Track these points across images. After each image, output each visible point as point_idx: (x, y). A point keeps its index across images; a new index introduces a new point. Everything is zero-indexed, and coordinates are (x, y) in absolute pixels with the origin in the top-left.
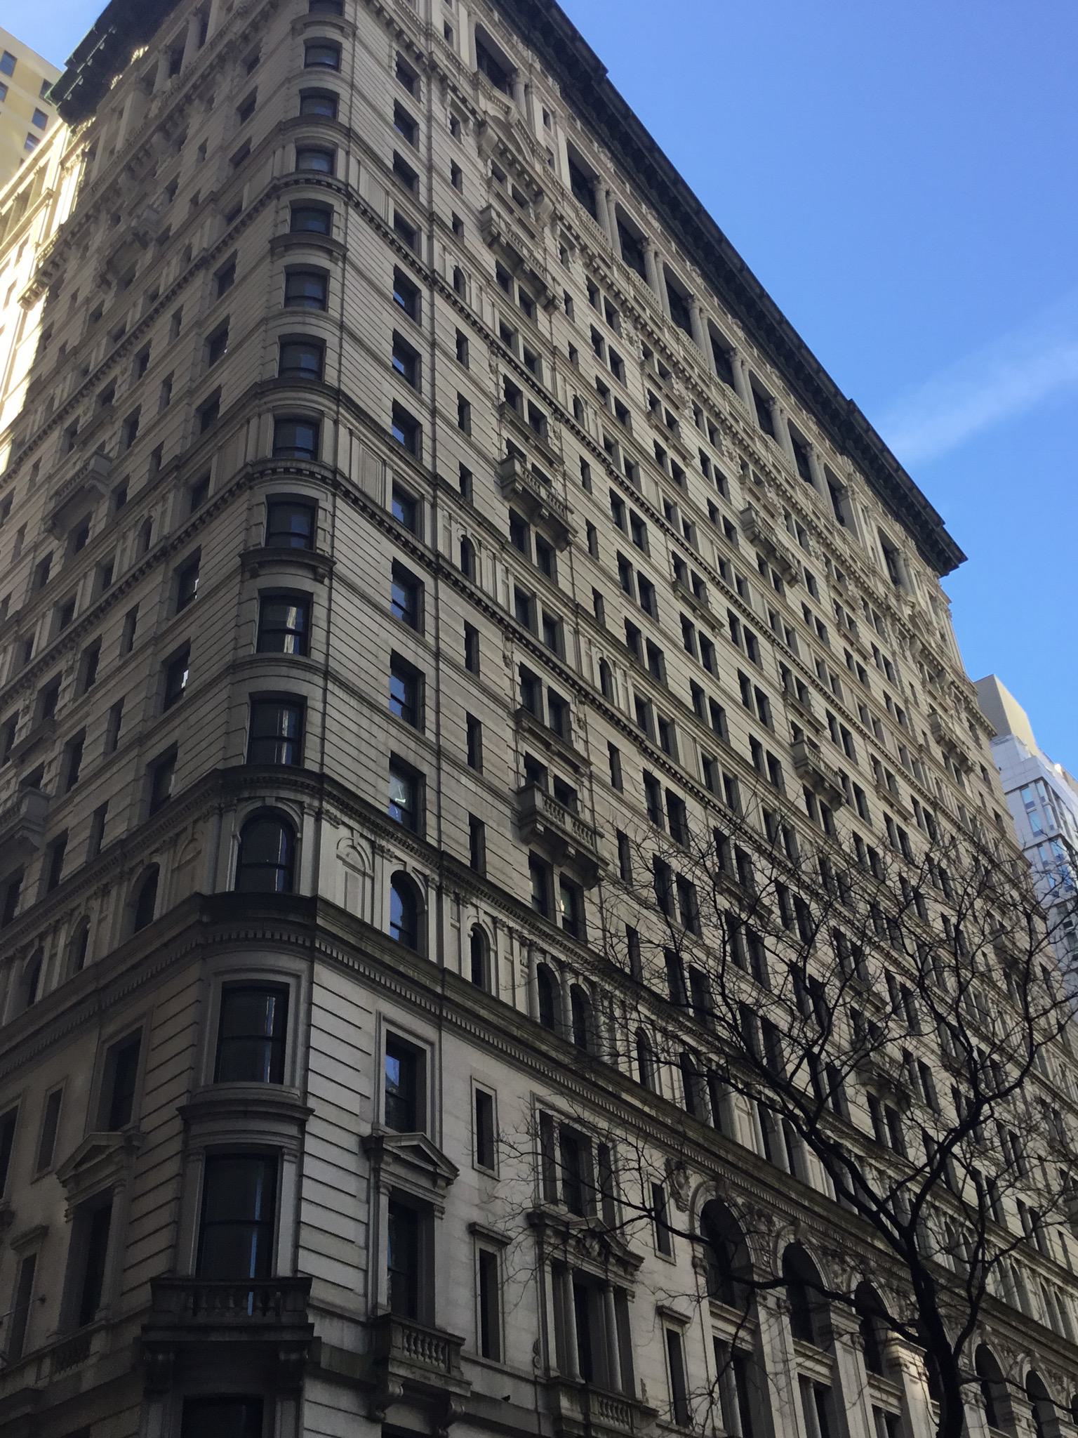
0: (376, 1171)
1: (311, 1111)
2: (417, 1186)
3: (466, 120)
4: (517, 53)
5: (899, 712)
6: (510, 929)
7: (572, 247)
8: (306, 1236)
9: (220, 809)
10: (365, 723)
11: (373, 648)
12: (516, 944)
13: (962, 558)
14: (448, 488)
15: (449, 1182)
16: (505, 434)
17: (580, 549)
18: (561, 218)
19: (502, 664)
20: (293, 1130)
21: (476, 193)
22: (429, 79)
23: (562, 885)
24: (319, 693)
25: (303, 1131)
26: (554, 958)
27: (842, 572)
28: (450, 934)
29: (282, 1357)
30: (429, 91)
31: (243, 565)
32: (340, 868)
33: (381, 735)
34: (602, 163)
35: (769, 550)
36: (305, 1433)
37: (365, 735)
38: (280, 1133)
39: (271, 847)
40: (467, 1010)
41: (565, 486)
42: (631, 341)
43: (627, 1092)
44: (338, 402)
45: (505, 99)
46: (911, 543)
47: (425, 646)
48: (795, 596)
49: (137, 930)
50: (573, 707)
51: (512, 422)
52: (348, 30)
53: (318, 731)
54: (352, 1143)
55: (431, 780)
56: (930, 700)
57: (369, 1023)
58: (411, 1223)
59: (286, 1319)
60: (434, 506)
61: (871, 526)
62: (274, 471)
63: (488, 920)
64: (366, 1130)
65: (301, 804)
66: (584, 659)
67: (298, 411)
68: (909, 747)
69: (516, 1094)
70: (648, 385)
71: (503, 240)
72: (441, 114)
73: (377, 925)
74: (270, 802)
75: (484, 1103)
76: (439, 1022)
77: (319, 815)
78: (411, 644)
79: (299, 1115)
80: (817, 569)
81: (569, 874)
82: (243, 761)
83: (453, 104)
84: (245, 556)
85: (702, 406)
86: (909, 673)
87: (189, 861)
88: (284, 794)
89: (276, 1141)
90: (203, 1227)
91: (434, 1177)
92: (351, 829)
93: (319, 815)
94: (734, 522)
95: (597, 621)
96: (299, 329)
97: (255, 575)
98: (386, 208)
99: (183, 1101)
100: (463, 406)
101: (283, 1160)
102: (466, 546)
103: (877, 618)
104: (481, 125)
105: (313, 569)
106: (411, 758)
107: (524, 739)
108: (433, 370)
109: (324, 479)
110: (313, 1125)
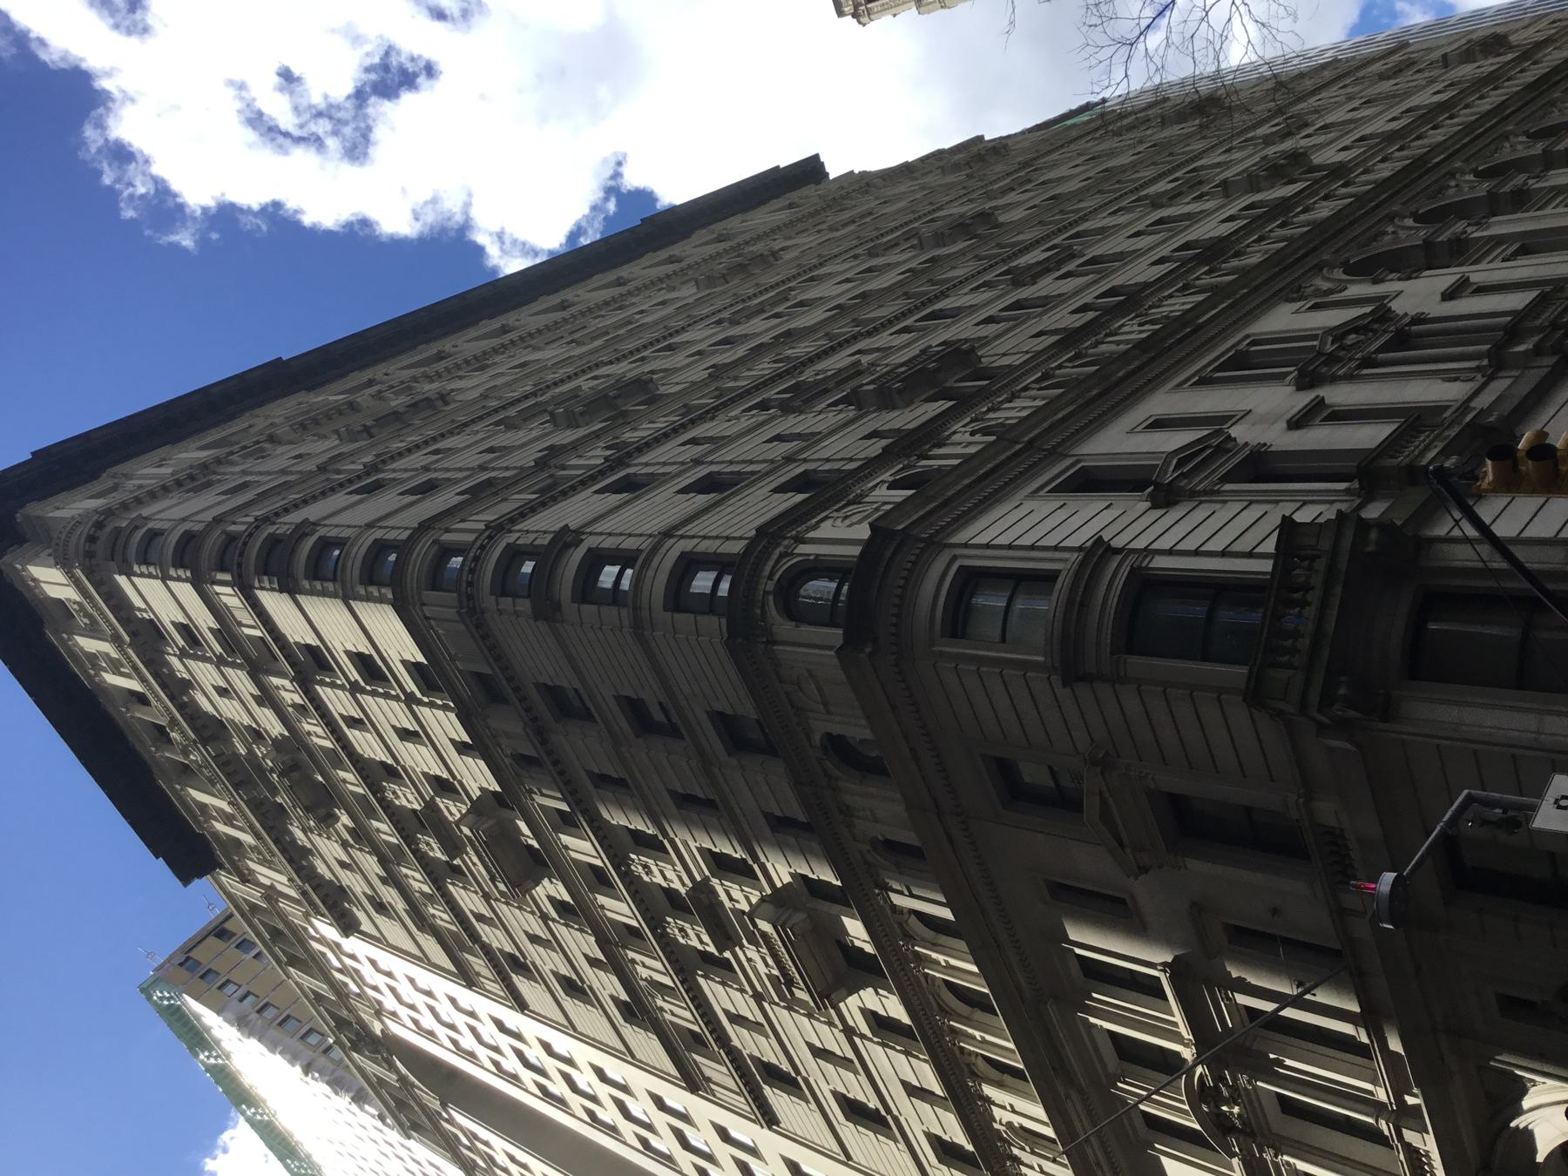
7: (410, 388)
9: (768, 642)
13: (816, 157)
22: (215, 473)
29: (1370, 548)
31: (546, 619)
38: (1115, 576)
40: (1051, 427)
41: (682, 537)
43: (1198, 317)
49: (888, 775)
52: (138, 523)
59: (1326, 545)
62: (470, 584)
65: (781, 556)
67: (425, 568)
71: (369, 423)
74: (770, 586)
82: (724, 621)
84: (538, 615)
87: (820, 689)
88: (768, 569)
90: (1206, 657)
92: (826, 518)
93: (801, 540)
96: (358, 563)
97: (558, 607)
99: (1056, 680)
101: (1147, 568)
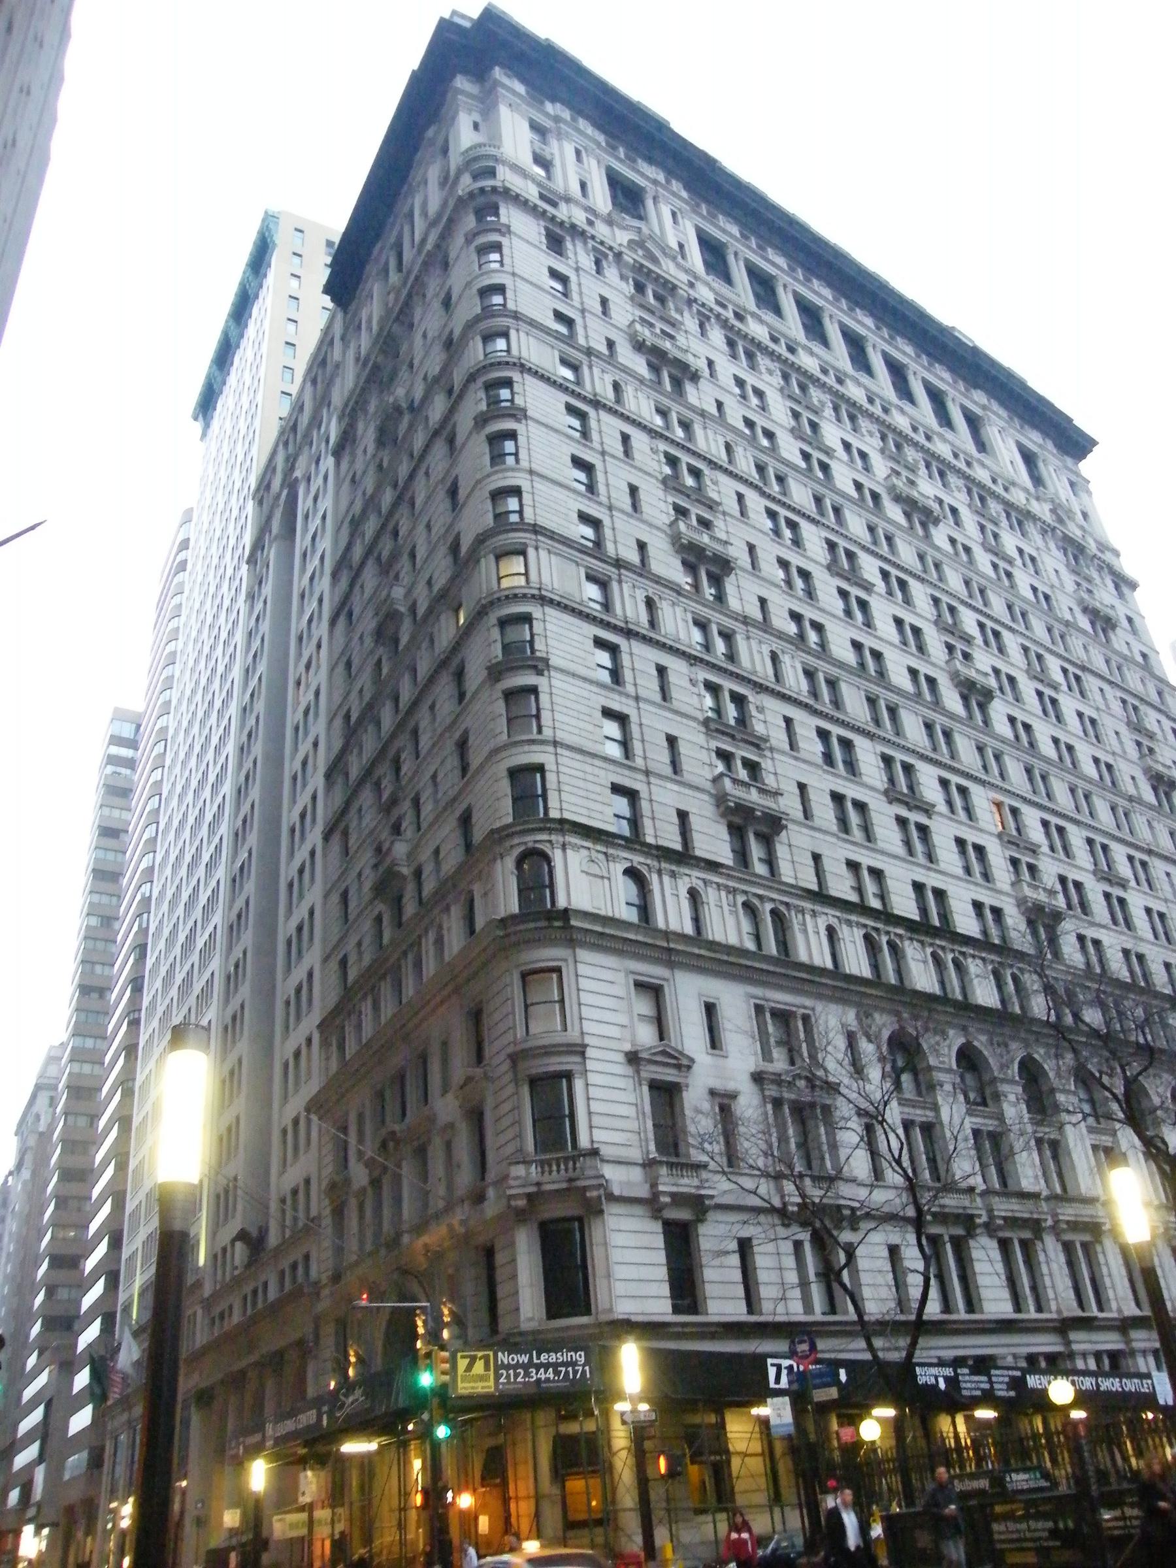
0: (638, 1072)
1: (586, 1046)
2: (669, 1075)
3: (606, 256)
4: (644, 174)
5: (1033, 559)
6: (718, 885)
7: (708, 318)
8: (596, 1120)
10: (589, 769)
11: (587, 711)
12: (723, 894)
14: (599, 355)
15: (689, 1067)
16: (670, 499)
17: (744, 570)
18: (695, 300)
19: (689, 685)
20: (577, 1059)
21: (624, 312)
23: (720, 633)
24: (552, 758)
25: (584, 1058)
26: (755, 895)
27: (980, 494)
28: (673, 913)
30: (661, 883)
32: (587, 884)
33: (602, 773)
34: (727, 230)
35: (911, 506)
36: (618, 1284)
37: (590, 778)
38: (567, 1063)
39: (535, 870)
42: (770, 372)
44: (536, 532)
45: (636, 223)
46: (1050, 445)
47: (628, 696)
48: (940, 535)
50: (751, 698)
51: (675, 489)
52: (520, 415)
53: (550, 723)
54: (620, 1058)
55: (644, 794)
56: (1074, 577)
57: (620, 977)
58: (666, 1095)
60: (590, 367)
61: (1006, 441)
63: (700, 883)
64: (627, 1047)
65: (550, 841)
66: (757, 657)
68: (1056, 625)
69: (736, 1002)
70: (789, 404)
72: (587, 261)
73: (617, 916)
75: (710, 1009)
76: (671, 965)
77: (564, 847)
78: (616, 697)
79: (580, 1050)
80: (959, 499)
81: (713, 569)
83: (594, 249)
85: (840, 401)
86: (1053, 560)
89: (568, 1067)
91: (678, 1067)
93: (564, 847)
94: (879, 489)
95: (765, 625)
98: (531, 192)
100: (604, 302)
102: (616, 386)
103: (1020, 523)
104: (618, 256)
105: (535, 667)
106: (615, 707)
107: (714, 738)
108: (585, 327)
109: (533, 596)
110: (590, 1053)
